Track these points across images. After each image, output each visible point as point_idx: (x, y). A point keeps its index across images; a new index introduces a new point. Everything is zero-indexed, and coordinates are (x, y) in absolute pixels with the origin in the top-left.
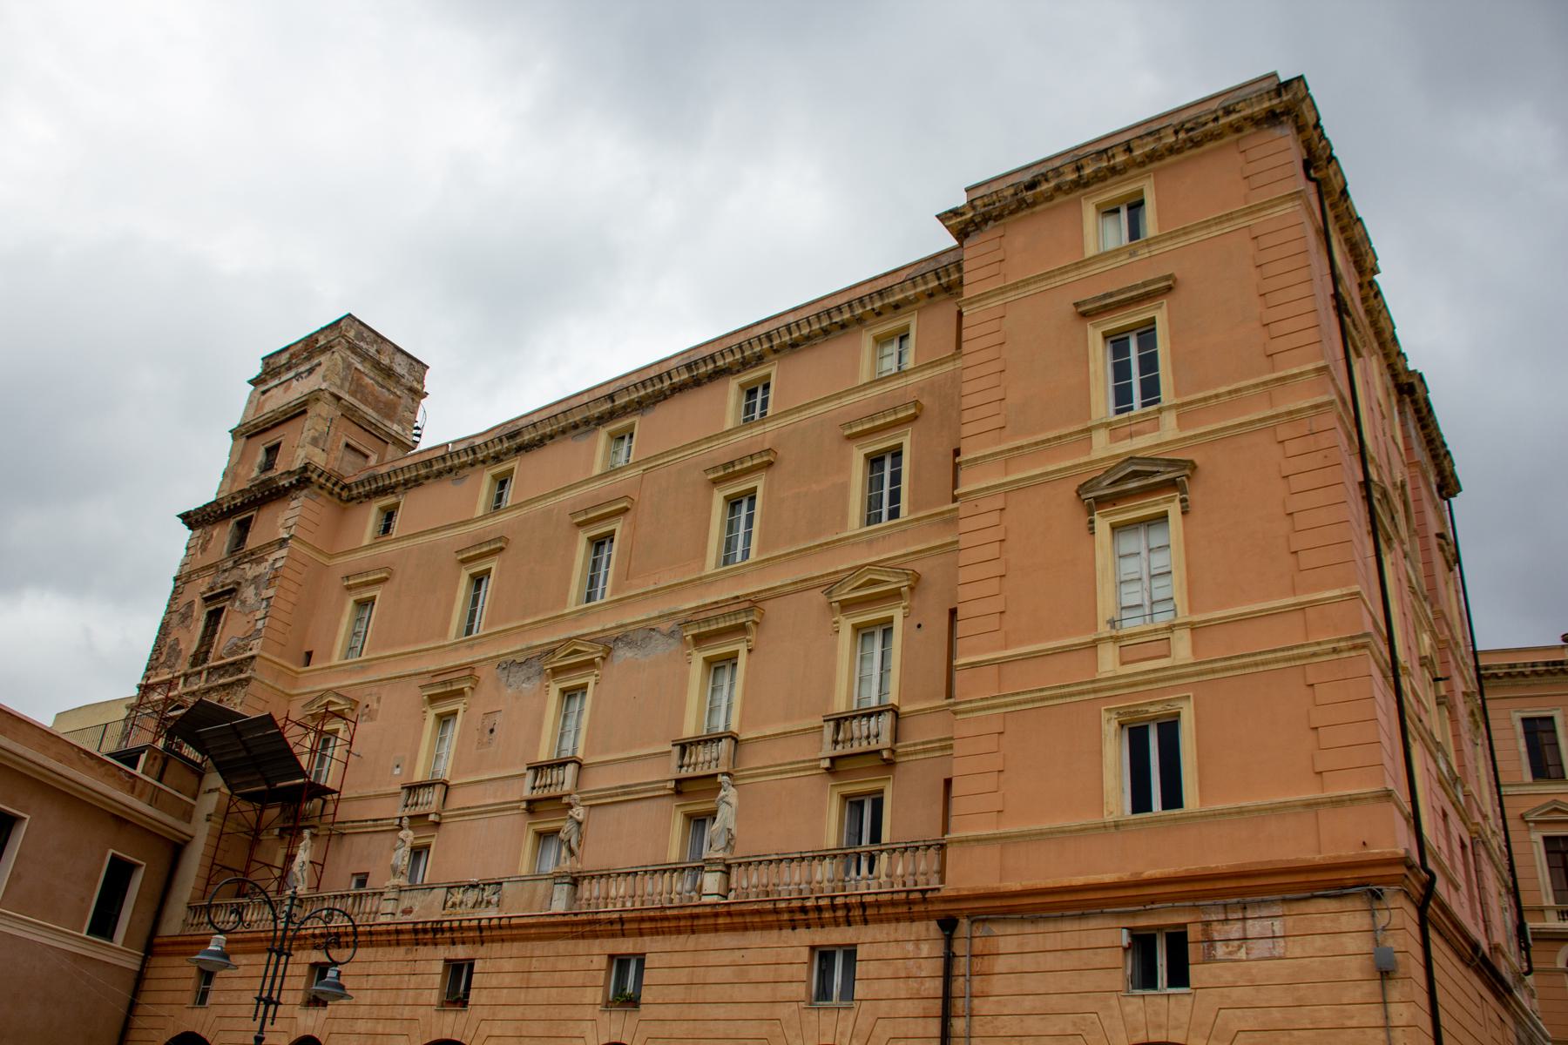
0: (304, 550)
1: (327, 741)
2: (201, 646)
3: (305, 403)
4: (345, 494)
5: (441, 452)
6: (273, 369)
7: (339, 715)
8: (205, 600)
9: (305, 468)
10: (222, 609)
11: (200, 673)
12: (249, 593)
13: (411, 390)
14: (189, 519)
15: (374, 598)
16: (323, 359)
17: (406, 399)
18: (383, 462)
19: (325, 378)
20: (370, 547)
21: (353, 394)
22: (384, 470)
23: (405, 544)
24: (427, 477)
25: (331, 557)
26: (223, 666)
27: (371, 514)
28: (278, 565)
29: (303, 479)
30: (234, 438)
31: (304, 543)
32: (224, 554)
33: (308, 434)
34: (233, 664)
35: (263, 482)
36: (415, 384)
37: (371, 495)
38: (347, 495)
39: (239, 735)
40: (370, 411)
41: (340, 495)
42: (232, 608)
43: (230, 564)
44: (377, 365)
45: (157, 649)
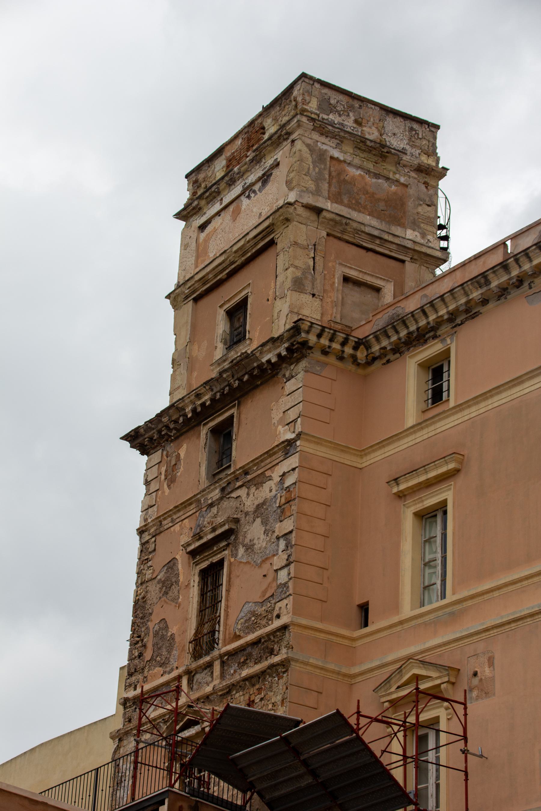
0: (322, 451)
1: (422, 740)
2: (201, 624)
3: (270, 230)
4: (361, 354)
5: (497, 258)
6: (207, 189)
7: (435, 695)
8: (192, 559)
9: (296, 329)
10: (221, 563)
11: (209, 665)
12: (254, 532)
13: (422, 170)
14: (141, 439)
15: (443, 505)
16: (279, 155)
17: (416, 188)
18: (402, 296)
19: (289, 184)
20: (418, 426)
21: (336, 198)
22: (411, 305)
23: (473, 412)
24: (485, 302)
25: (363, 453)
26: (241, 649)
27: (409, 376)
28: (289, 481)
29: (296, 346)
30: (175, 305)
31: (319, 441)
32: (204, 483)
33: (286, 277)
34: (256, 643)
35: (236, 364)
36: (425, 160)
37: (399, 349)
38: (365, 355)
39: (296, 752)
40: (367, 219)
41: (354, 358)
42: (235, 559)
43: (216, 494)
44: (361, 144)
45: (137, 640)
